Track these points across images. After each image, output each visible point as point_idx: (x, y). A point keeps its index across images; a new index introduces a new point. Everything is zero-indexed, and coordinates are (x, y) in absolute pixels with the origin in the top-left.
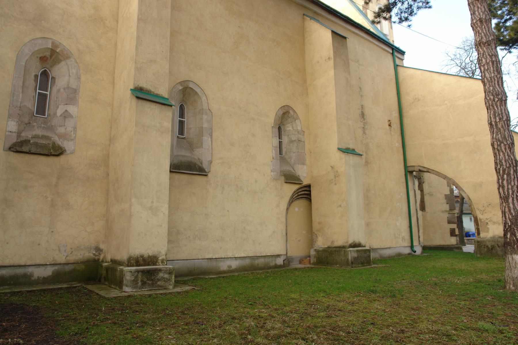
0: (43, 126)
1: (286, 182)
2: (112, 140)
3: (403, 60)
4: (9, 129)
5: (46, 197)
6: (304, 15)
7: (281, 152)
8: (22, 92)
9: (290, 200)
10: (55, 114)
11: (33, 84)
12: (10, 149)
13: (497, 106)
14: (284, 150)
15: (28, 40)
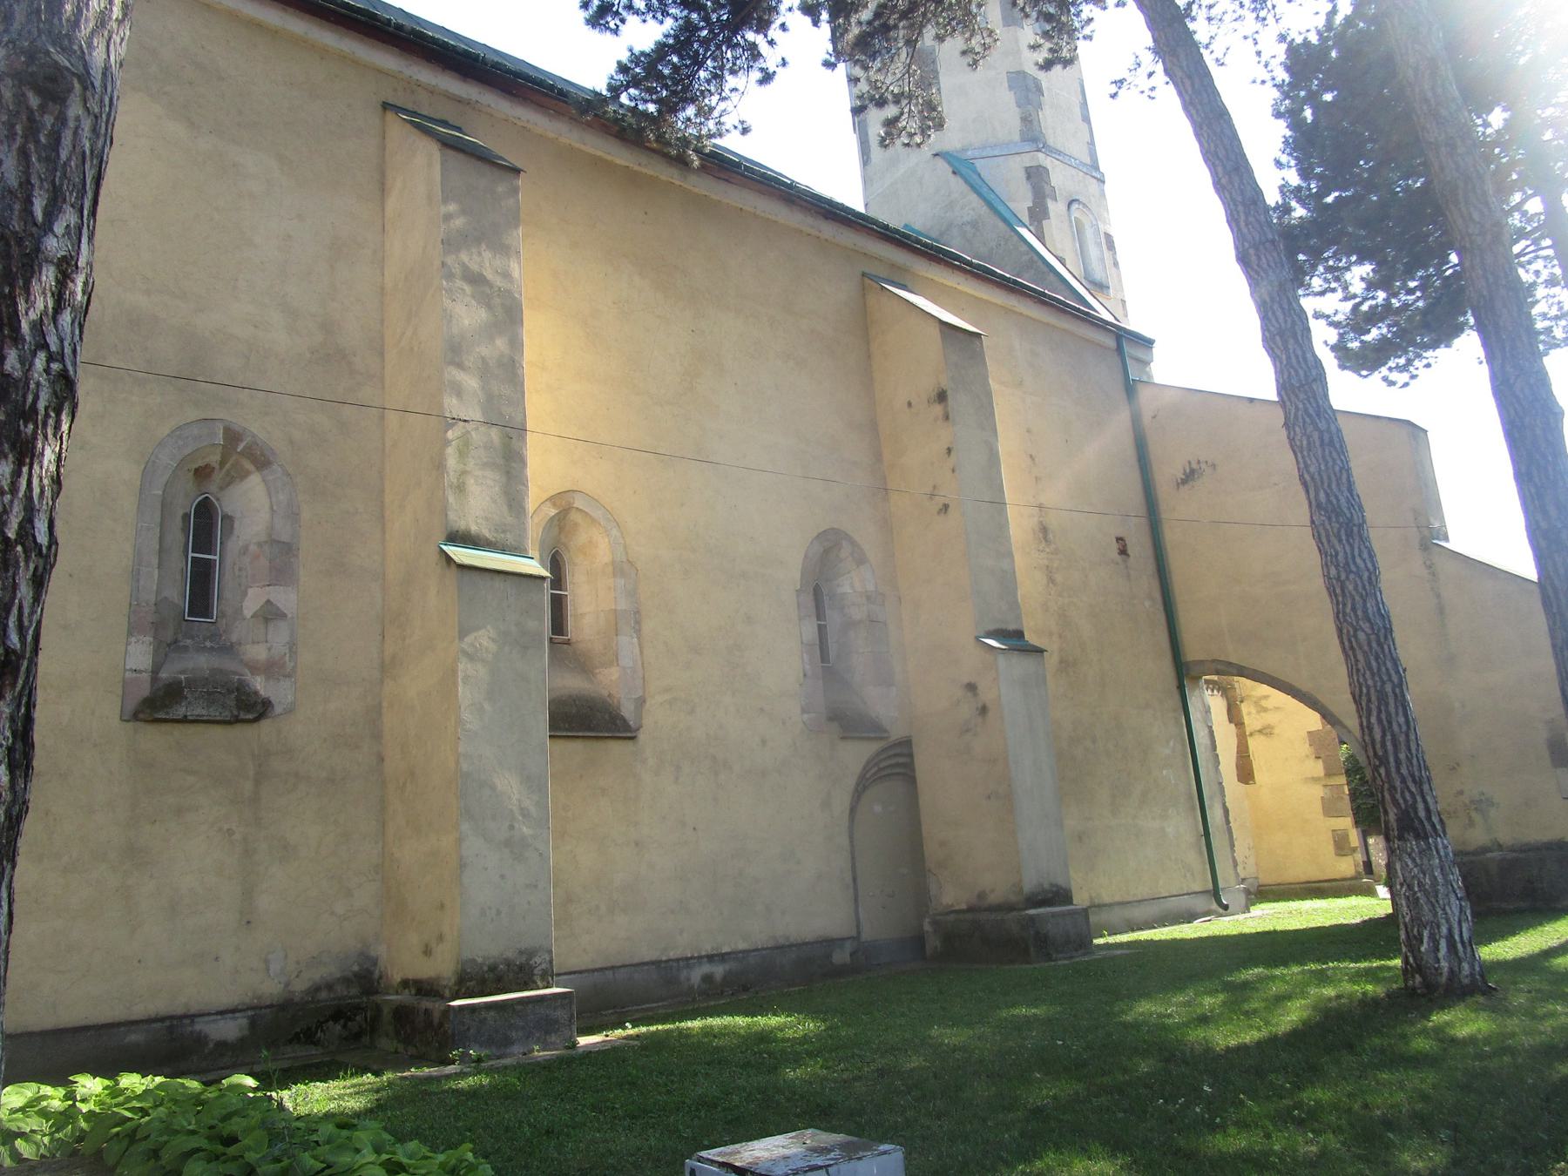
0: (208, 644)
1: (843, 738)
2: (387, 668)
3: (1147, 363)
4: (131, 664)
5: (230, 832)
6: (864, 275)
7: (824, 657)
8: (160, 566)
9: (858, 784)
10: (239, 610)
11: (180, 537)
12: (135, 716)
13: (1340, 541)
14: (832, 654)
15: (167, 432)
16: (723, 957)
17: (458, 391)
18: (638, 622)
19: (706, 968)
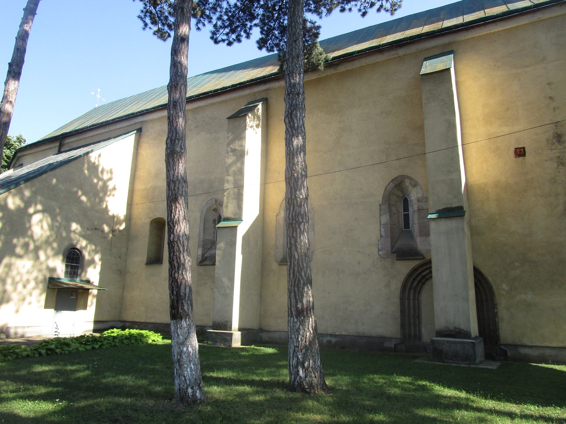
16: (335, 336)
17: (228, 181)
18: (314, 227)
19: (329, 338)
